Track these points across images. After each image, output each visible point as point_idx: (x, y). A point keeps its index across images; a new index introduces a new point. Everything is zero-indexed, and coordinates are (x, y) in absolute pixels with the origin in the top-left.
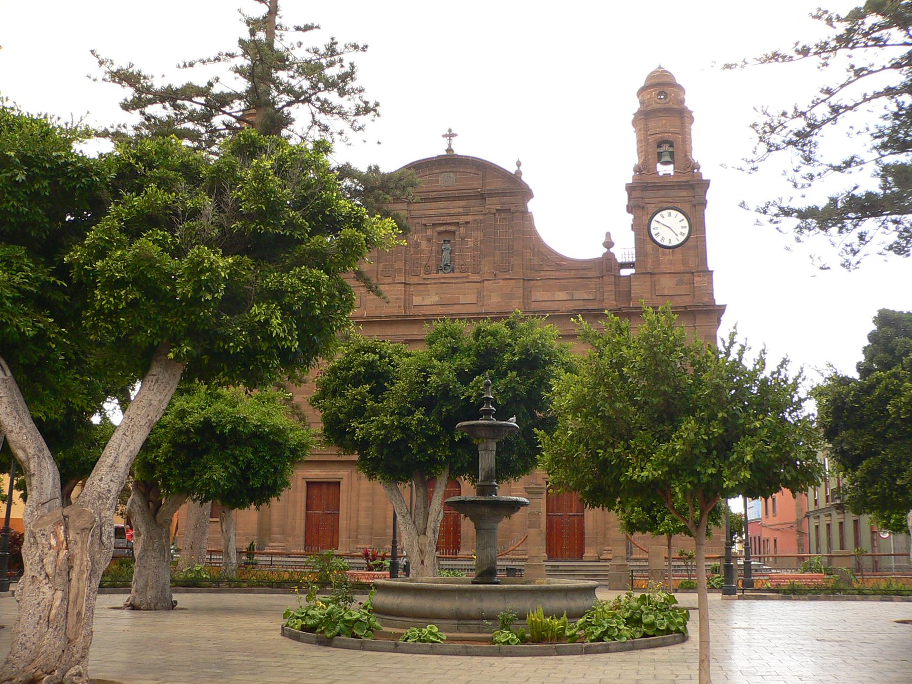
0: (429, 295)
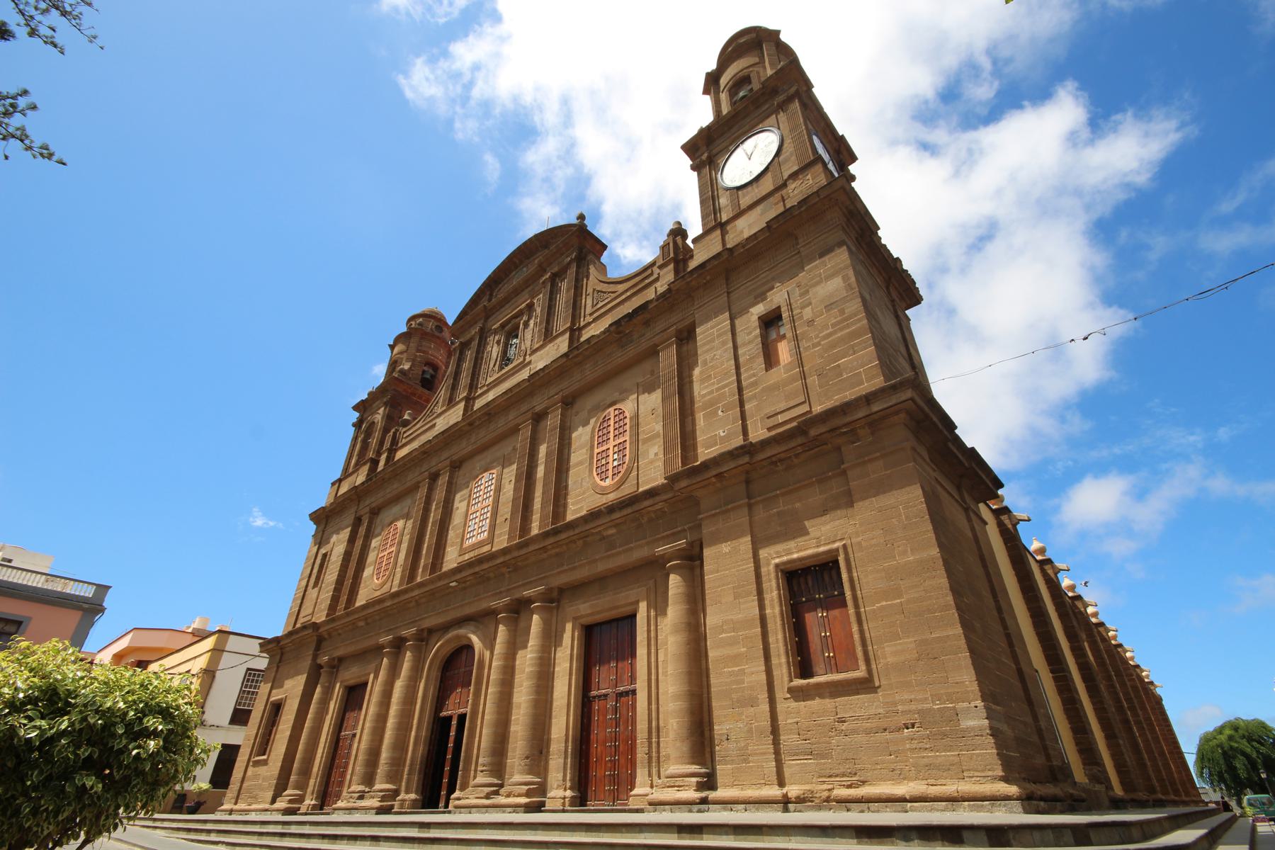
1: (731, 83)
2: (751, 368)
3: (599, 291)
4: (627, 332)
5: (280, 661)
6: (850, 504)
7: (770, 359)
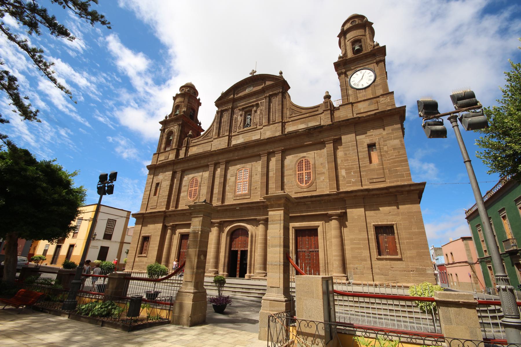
0: (239, 139)
1: (352, 39)
2: (364, 161)
3: (292, 109)
5: (143, 222)
6: (55, 79)
7: (155, 194)
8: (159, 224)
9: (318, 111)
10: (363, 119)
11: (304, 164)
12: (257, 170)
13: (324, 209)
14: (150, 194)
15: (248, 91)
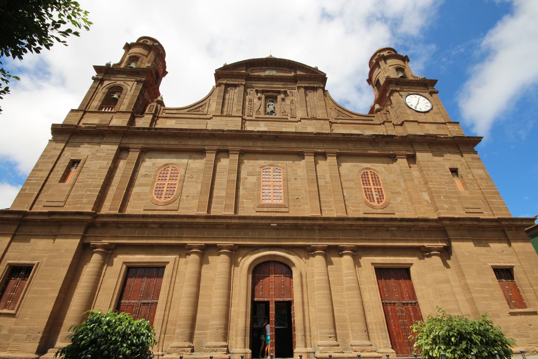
0: (259, 126)
4: (377, 141)
7: (64, 179)
8: (69, 241)
9: (372, 120)
10: (440, 139)
11: (370, 176)
12: (297, 174)
13: (381, 239)
14: (48, 178)
15: (268, 73)
